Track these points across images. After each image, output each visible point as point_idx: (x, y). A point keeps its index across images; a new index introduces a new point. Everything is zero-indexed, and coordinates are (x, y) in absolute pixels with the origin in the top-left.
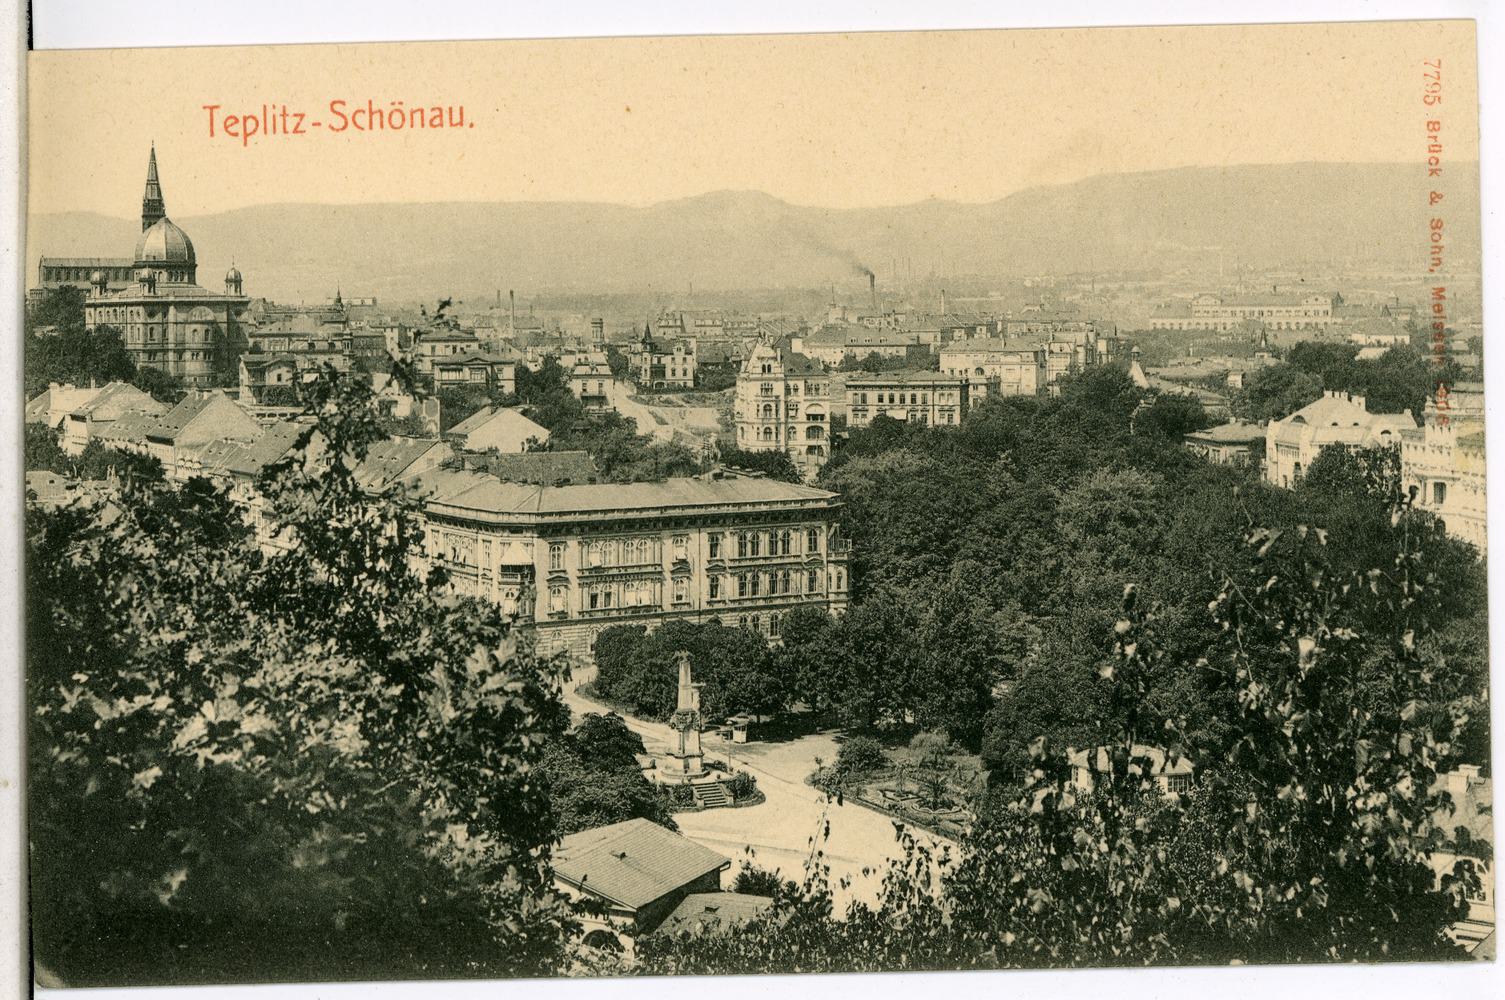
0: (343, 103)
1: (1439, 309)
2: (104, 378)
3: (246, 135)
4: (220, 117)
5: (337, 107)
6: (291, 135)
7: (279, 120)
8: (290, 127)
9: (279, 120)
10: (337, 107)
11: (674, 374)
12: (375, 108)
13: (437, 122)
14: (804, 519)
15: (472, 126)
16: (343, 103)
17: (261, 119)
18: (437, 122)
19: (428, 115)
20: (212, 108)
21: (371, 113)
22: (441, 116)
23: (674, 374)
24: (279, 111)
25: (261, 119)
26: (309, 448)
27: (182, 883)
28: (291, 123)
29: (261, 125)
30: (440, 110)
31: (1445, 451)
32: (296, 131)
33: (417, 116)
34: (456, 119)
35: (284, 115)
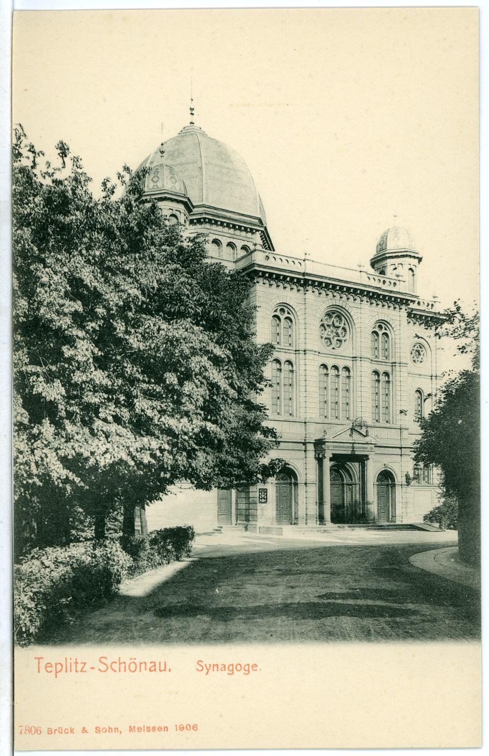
4: (43, 663)
5: (200, 663)
10: (200, 663)
24: (73, 661)
28: (80, 667)
34: (162, 668)
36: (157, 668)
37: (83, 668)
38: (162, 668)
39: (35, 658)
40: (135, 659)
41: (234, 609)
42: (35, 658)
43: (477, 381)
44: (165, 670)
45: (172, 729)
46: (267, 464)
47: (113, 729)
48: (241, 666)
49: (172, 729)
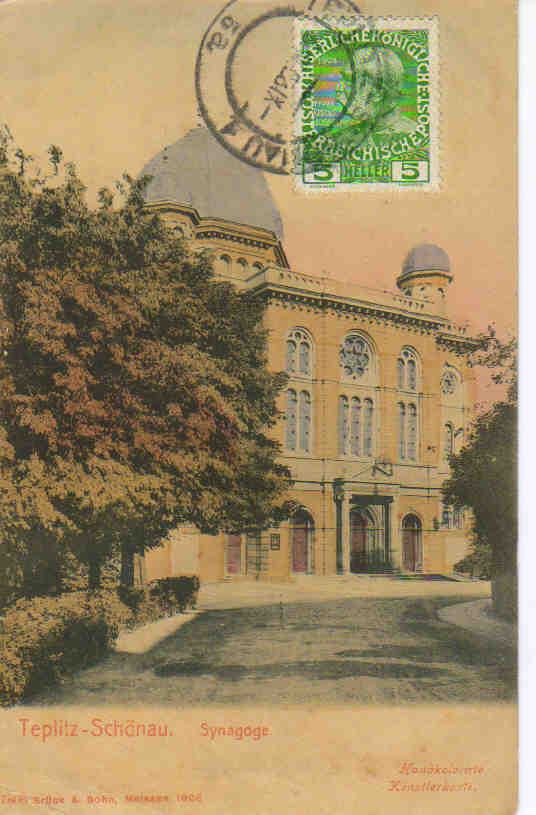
0: (99, 720)
2: (24, 394)
3: (44, 736)
8: (69, 732)
13: (151, 733)
15: (171, 735)
16: (99, 720)
17: (220, 20)
18: (151, 733)
19: (147, 728)
20: (24, 720)
22: (154, 729)
24: (64, 724)
25: (220, 20)
26: (347, 394)
29: (222, 17)
30: (154, 726)
31: (466, 411)
32: (72, 735)
35: (66, 726)
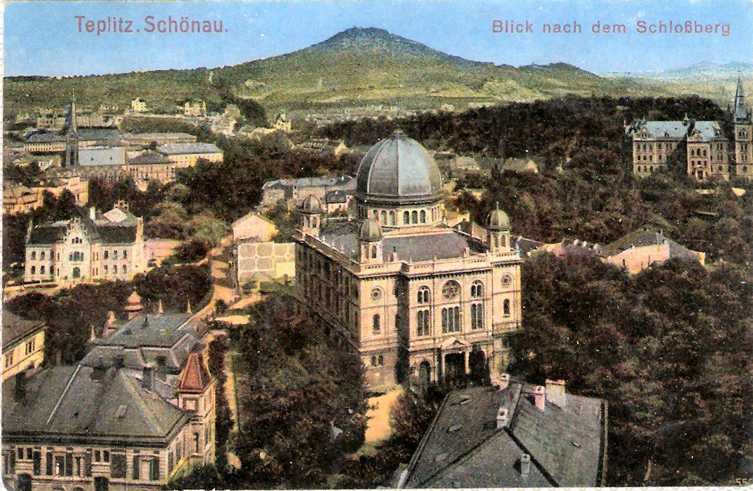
0: (153, 18)
1: (624, 264)
4: (84, 22)
5: (149, 20)
6: (124, 33)
7: (118, 24)
9: (118, 24)
10: (149, 20)
11: (43, 253)
12: (173, 19)
14: (51, 468)
16: (153, 18)
18: (207, 29)
19: (202, 25)
21: (170, 22)
22: (93, 25)
23: (43, 253)
24: (117, 19)
27: (552, 255)
28: (124, 26)
33: (196, 26)
34: (218, 28)
36: (213, 29)
37: (128, 28)
38: (218, 28)
39: (599, 22)
40: (186, 18)
41: (732, 147)
42: (599, 22)
43: (6, 229)
44: (221, 30)
45: (587, 29)
46: (557, 255)
47: (552, 28)
48: (517, 30)
49: (587, 29)
